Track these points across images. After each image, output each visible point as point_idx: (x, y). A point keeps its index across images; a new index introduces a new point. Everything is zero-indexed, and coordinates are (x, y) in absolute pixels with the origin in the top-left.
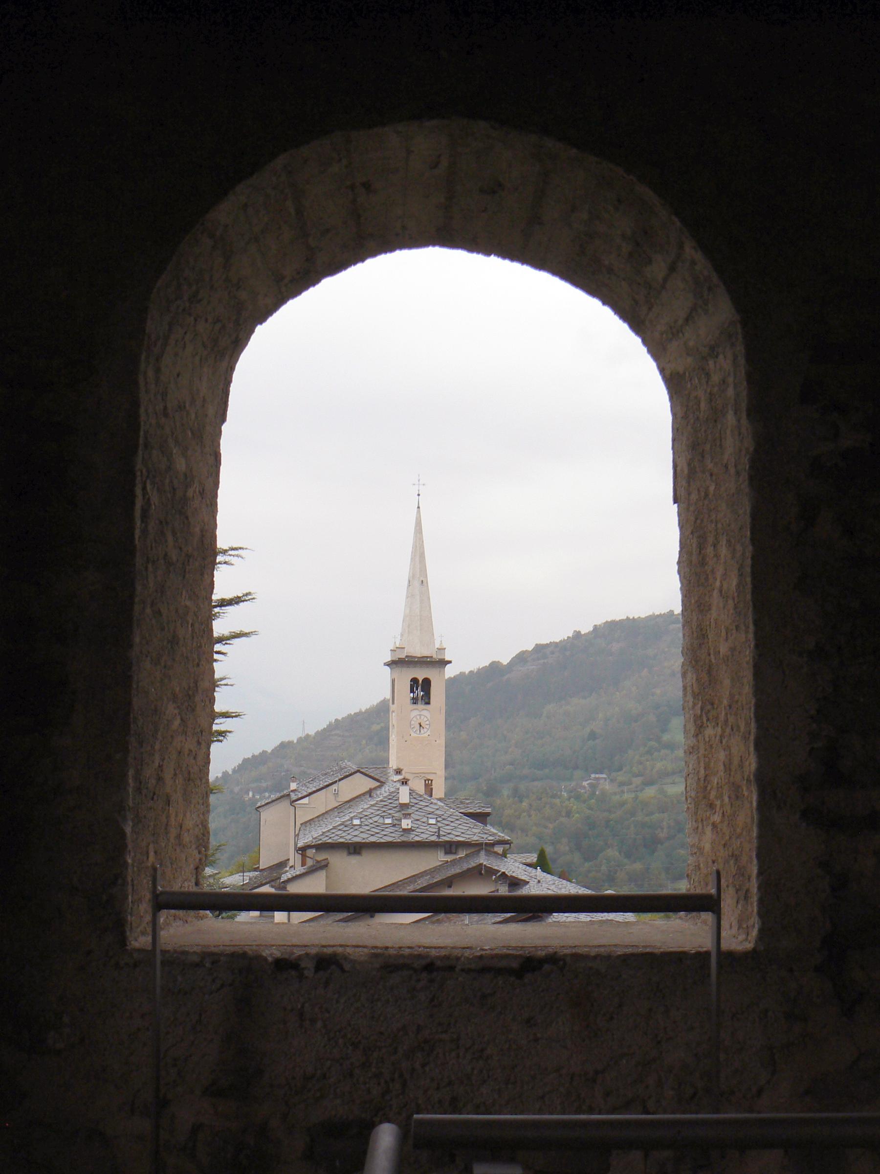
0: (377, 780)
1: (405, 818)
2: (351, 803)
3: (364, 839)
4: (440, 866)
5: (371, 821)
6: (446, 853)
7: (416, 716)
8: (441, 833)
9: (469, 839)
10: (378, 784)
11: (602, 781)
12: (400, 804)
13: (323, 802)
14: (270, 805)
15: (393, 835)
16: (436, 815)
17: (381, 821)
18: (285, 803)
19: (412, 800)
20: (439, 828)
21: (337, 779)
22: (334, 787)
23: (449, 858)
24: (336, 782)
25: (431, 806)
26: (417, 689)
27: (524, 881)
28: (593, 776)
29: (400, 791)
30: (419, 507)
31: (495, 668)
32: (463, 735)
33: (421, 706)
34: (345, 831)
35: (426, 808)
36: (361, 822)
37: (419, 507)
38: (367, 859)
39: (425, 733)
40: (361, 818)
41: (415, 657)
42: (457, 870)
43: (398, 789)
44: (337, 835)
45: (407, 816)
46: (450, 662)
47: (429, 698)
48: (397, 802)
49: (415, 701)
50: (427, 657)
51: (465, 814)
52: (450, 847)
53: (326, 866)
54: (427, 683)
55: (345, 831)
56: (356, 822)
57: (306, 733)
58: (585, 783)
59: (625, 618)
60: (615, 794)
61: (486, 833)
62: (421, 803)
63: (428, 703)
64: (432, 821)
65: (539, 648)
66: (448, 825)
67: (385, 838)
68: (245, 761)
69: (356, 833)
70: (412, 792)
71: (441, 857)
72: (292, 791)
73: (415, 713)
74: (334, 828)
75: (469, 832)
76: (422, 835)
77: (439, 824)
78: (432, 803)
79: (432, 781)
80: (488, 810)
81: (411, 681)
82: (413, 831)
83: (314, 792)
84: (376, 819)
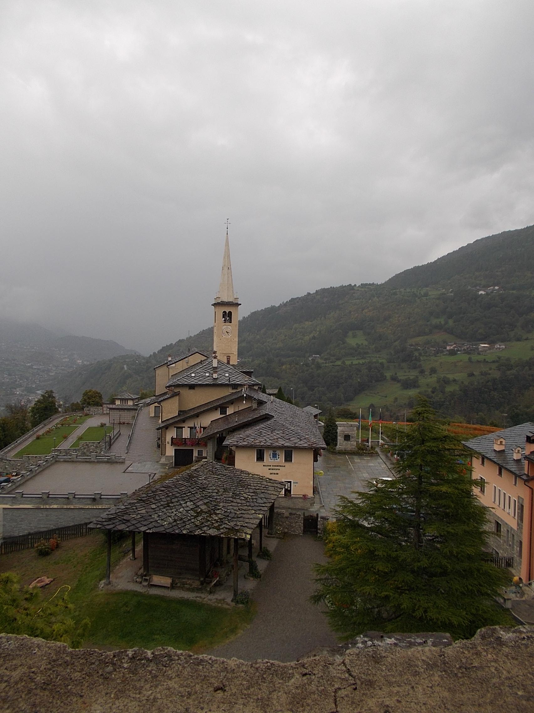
0: (206, 356)
5: (199, 375)
6: (233, 389)
11: (317, 358)
13: (180, 366)
22: (187, 359)
23: (234, 391)
24: (187, 357)
28: (313, 356)
31: (273, 309)
38: (198, 391)
42: (234, 397)
45: (215, 372)
46: (241, 304)
47: (231, 320)
51: (244, 372)
52: (235, 386)
53: (179, 394)
54: (230, 313)
56: (193, 375)
63: (231, 322)
64: (227, 375)
65: (292, 300)
68: (163, 347)
69: (193, 380)
70: (219, 362)
71: (231, 391)
73: (225, 327)
74: (183, 377)
76: (222, 381)
77: (230, 376)
80: (252, 370)
83: (177, 362)
84: (202, 374)
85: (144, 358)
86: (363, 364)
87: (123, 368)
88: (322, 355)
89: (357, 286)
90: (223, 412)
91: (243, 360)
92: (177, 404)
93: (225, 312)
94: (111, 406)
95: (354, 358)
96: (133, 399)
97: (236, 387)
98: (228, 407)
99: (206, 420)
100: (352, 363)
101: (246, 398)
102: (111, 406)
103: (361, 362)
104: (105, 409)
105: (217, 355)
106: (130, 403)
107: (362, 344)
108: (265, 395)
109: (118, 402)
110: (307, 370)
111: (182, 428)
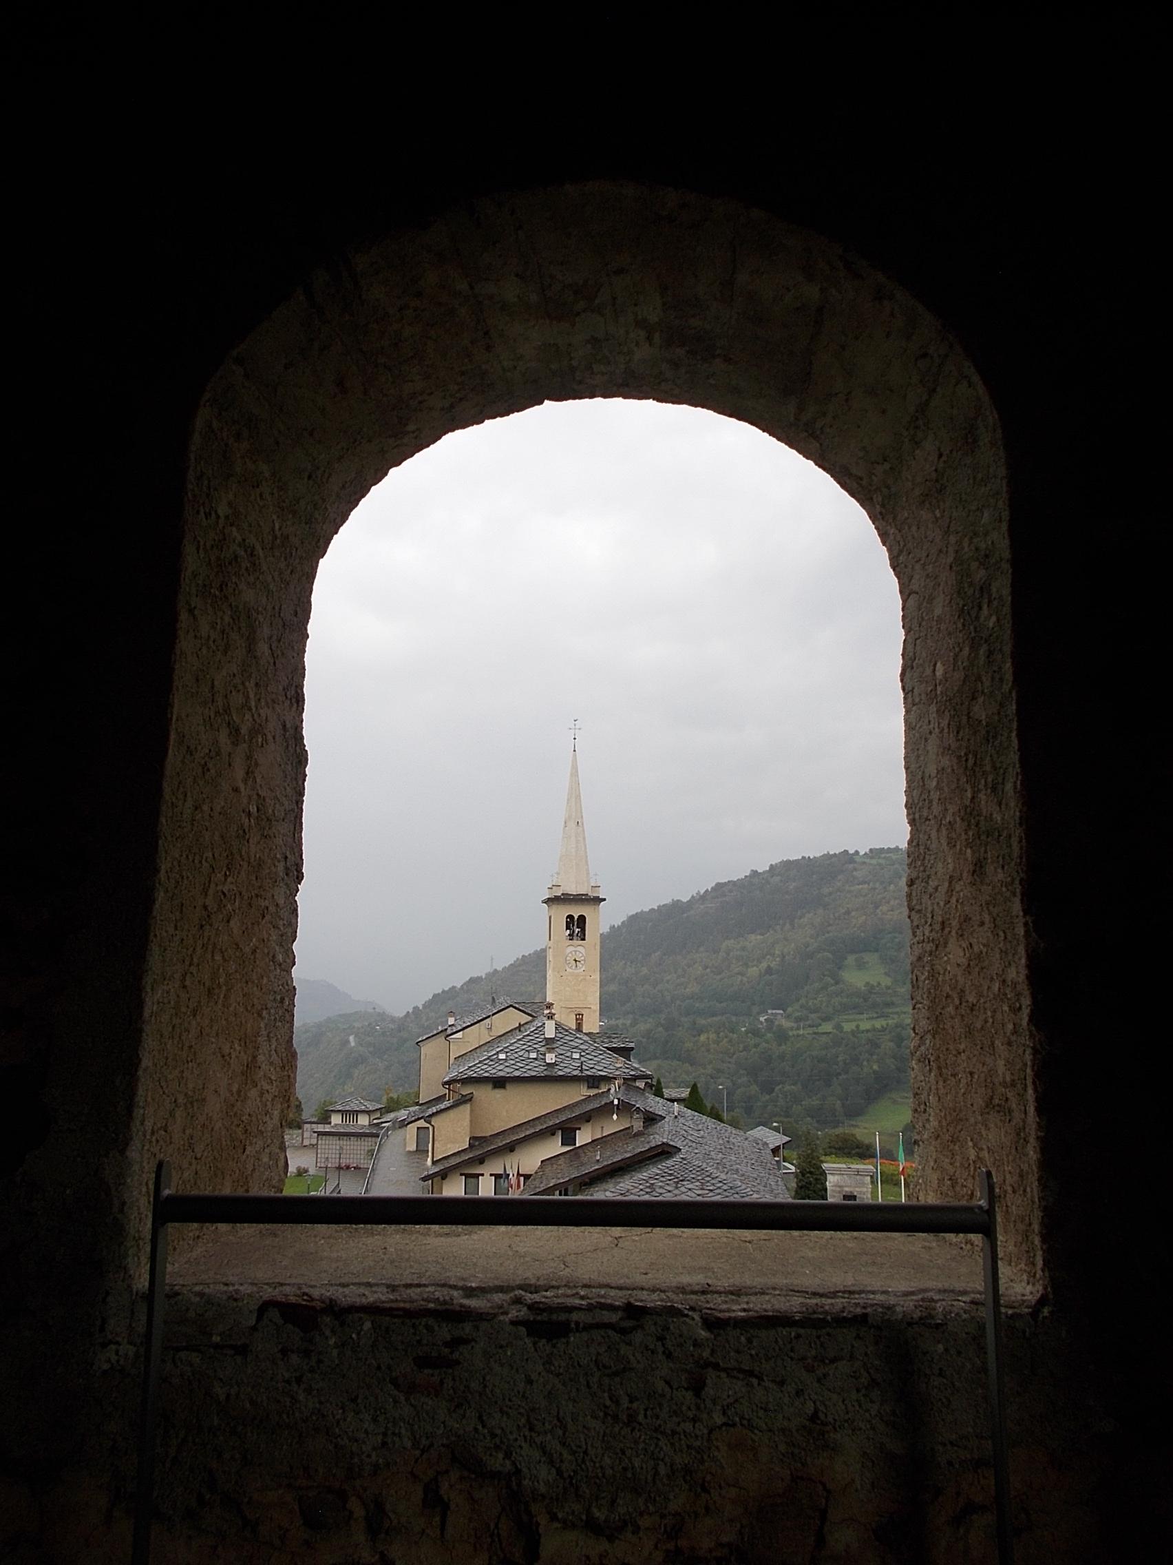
1: (549, 1052)
2: (502, 1038)
3: (508, 1073)
4: (583, 1100)
5: (516, 1055)
7: (571, 952)
8: (584, 1067)
9: (611, 1073)
10: (530, 1018)
11: (779, 1017)
12: (545, 1038)
13: (476, 1036)
14: (430, 1039)
15: (537, 1069)
16: (580, 1049)
17: (526, 1055)
18: (441, 1039)
19: (558, 1035)
20: (582, 1063)
21: (491, 1014)
23: (592, 1092)
24: (489, 1016)
25: (576, 1040)
26: (573, 926)
27: (660, 1116)
28: (770, 1011)
29: (546, 1025)
30: (575, 751)
31: (676, 905)
32: (645, 971)
33: (576, 942)
34: (490, 1066)
35: (571, 1043)
36: (507, 1056)
37: (575, 751)
38: (511, 1091)
39: (581, 968)
40: (507, 1052)
41: (571, 895)
43: (544, 1024)
44: (482, 1070)
45: (551, 1050)
46: (604, 900)
47: (584, 935)
48: (543, 1037)
49: (571, 936)
50: (583, 895)
52: (594, 1081)
53: (470, 1100)
54: (582, 919)
55: (490, 1066)
56: (502, 1056)
57: (494, 968)
58: (762, 1019)
59: (800, 858)
60: (792, 1029)
61: (628, 1068)
62: (567, 1038)
63: (583, 939)
64: (576, 1056)
65: (719, 886)
66: (591, 1059)
67: (528, 1072)
69: (501, 1067)
70: (558, 1026)
71: (584, 1091)
72: (450, 1026)
73: (571, 949)
74: (480, 1062)
75: (611, 1067)
76: (565, 1070)
77: (583, 1059)
78: (577, 1038)
79: (582, 1015)
80: (632, 1045)
81: (567, 918)
82: (557, 1065)
85: (393, 1020)
86: (884, 1029)
87: (348, 1042)
88: (790, 1009)
89: (862, 853)
90: (569, 1139)
91: (613, 1022)
92: (466, 1123)
93: (570, 917)
94: (321, 1128)
95: (861, 1017)
96: (368, 1112)
97: (596, 1083)
98: (579, 1129)
99: (531, 1159)
100: (858, 1027)
101: (618, 1109)
102: (321, 1128)
103: (879, 1024)
104: (306, 1135)
105: (553, 1011)
106: (363, 1120)
107: (879, 984)
108: (661, 1101)
109: (336, 1119)
110: (756, 1046)
111: (477, 1176)
